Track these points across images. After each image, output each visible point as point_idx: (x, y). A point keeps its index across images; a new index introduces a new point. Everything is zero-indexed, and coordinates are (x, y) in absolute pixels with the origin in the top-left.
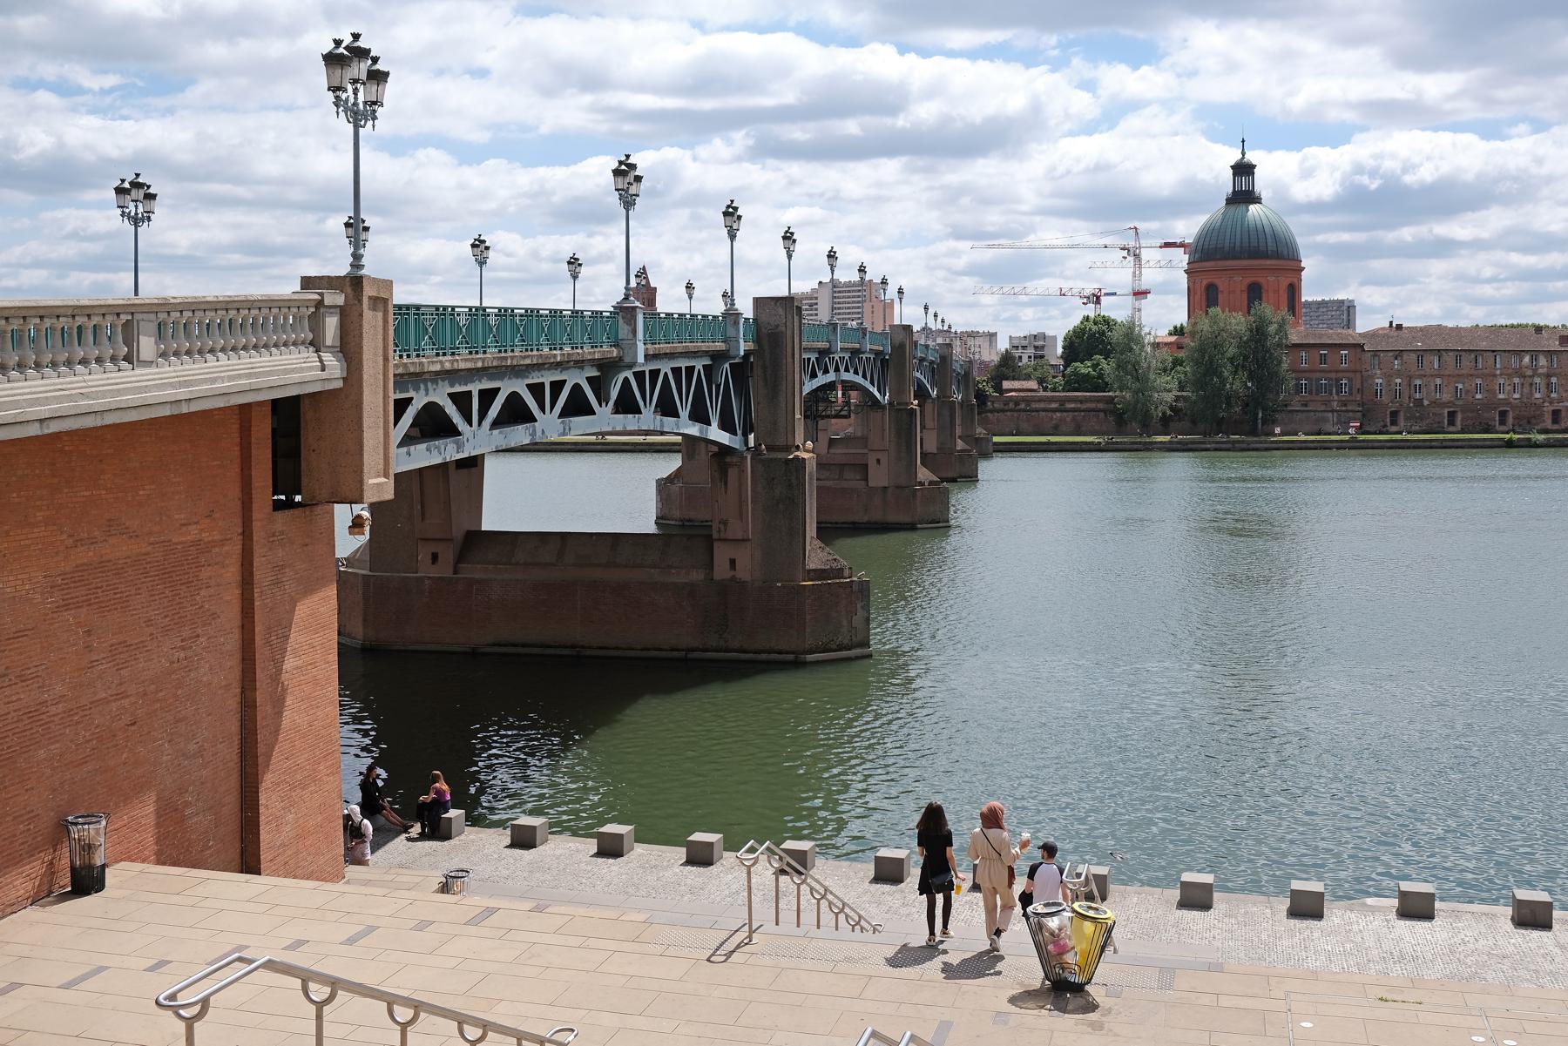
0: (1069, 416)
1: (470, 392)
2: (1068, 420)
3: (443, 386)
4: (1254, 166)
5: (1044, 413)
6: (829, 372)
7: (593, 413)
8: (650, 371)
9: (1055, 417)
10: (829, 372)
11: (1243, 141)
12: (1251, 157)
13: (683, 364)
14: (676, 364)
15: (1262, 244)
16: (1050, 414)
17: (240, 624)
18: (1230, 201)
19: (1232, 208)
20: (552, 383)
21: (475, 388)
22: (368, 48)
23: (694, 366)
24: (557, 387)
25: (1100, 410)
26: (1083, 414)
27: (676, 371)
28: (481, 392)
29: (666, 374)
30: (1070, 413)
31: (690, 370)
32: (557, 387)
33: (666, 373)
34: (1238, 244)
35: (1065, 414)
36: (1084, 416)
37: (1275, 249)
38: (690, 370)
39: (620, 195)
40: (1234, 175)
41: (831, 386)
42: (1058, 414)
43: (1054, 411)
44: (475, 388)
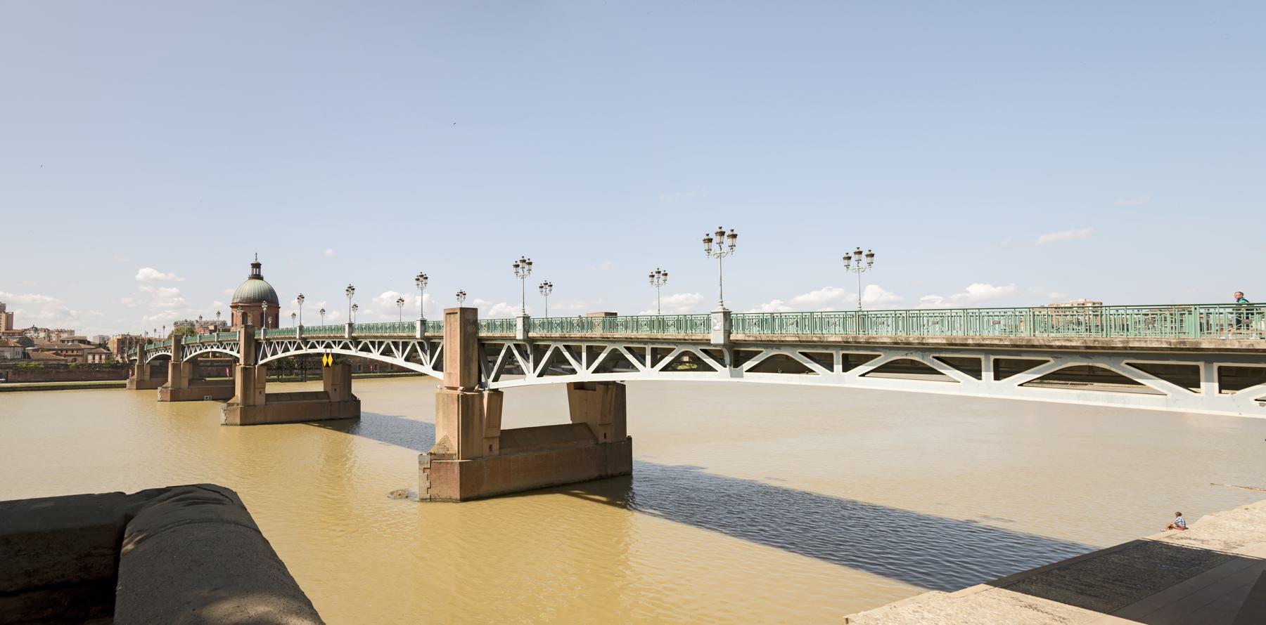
0: (214, 369)
8: (403, 342)
12: (259, 261)
24: (282, 343)
41: (209, 352)
42: (210, 368)
43: (208, 366)
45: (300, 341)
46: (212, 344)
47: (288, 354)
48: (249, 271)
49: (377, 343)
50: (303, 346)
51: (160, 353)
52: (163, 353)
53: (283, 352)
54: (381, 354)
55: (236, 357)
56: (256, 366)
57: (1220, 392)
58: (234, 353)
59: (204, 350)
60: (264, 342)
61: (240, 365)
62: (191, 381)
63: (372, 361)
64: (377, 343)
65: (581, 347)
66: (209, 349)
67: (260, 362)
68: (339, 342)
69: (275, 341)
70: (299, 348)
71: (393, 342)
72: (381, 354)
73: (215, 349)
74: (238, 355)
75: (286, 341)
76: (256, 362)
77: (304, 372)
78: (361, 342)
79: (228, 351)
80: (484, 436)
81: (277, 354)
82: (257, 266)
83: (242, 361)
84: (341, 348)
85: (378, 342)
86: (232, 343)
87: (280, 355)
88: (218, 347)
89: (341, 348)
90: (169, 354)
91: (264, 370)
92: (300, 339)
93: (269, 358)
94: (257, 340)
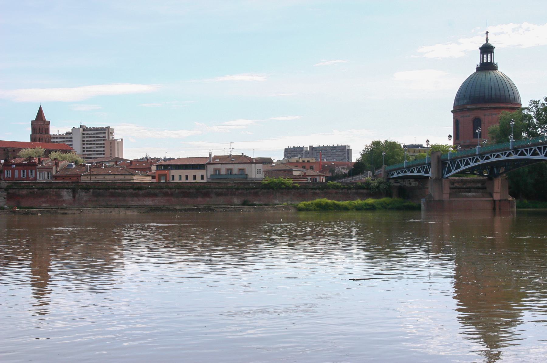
1: (541, 147)
4: (493, 48)
7: (526, 156)
15: (507, 94)
18: (479, 69)
19: (479, 73)
22: (494, 46)
24: (464, 160)
28: (529, 149)
34: (493, 94)
37: (514, 97)
40: (481, 53)
45: (478, 157)
48: (477, 60)
49: (493, 155)
57: (122, 139)
65: (541, 147)
68: (505, 153)
71: (459, 160)
82: (487, 49)
85: (529, 149)
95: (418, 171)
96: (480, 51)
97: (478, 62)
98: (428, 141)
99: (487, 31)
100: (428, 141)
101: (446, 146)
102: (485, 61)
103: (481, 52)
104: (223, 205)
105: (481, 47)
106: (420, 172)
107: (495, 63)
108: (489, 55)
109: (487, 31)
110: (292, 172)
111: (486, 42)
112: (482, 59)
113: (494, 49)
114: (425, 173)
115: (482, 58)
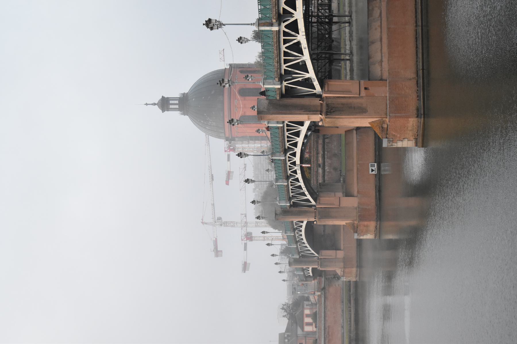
2: (330, 161)
3: (295, 300)
5: (326, 177)
6: (302, 238)
8: (287, 127)
9: (328, 170)
10: (302, 238)
11: (147, 104)
13: (288, 168)
14: (286, 141)
16: (326, 173)
17: (353, 37)
20: (287, 138)
21: (283, 58)
22: (161, 97)
23: (285, 85)
25: (324, 142)
26: (326, 153)
27: (288, 130)
29: (288, 134)
30: (326, 160)
31: (292, 189)
32: (286, 54)
33: (288, 134)
35: (326, 164)
36: (328, 152)
38: (292, 189)
39: (219, 28)
41: (302, 168)
42: (326, 168)
44: (282, 38)
45: (283, 25)
46: (288, 163)
47: (304, 44)
49: (289, 159)
50: (292, 20)
51: (303, 237)
52: (303, 233)
53: (299, 182)
54: (295, 157)
55: (309, 129)
56: (324, 95)
58: (303, 130)
59: (299, 176)
60: (285, 83)
61: (321, 120)
62: (348, 194)
63: (312, 59)
64: (289, 159)
66: (297, 168)
67: (318, 89)
69: (284, 67)
70: (294, 26)
71: (285, 64)
72: (295, 157)
73: (297, 159)
74: (307, 124)
75: (283, 48)
76: (319, 96)
77: (335, 19)
78: (283, 8)
79: (300, 140)
80: (359, 96)
81: (304, 62)
83: (317, 118)
84: (295, 10)
86: (287, 134)
87: (306, 57)
88: (294, 155)
89: (295, 10)
90: (304, 225)
91: (333, 84)
92: (279, 25)
93: (311, 74)
94: (282, 96)
95: (287, 86)
96: (166, 112)
97: (177, 113)
98: (268, 170)
99: (145, 104)
100: (268, 170)
101: (257, 41)
102: (171, 102)
103: (166, 111)
104: (319, 178)
105: (161, 111)
106: (297, 143)
107: (179, 96)
108: (171, 102)
109: (145, 104)
110: (313, 320)
111: (156, 106)
112: (173, 99)
113: (164, 97)
114: (299, 137)
115: (174, 99)
